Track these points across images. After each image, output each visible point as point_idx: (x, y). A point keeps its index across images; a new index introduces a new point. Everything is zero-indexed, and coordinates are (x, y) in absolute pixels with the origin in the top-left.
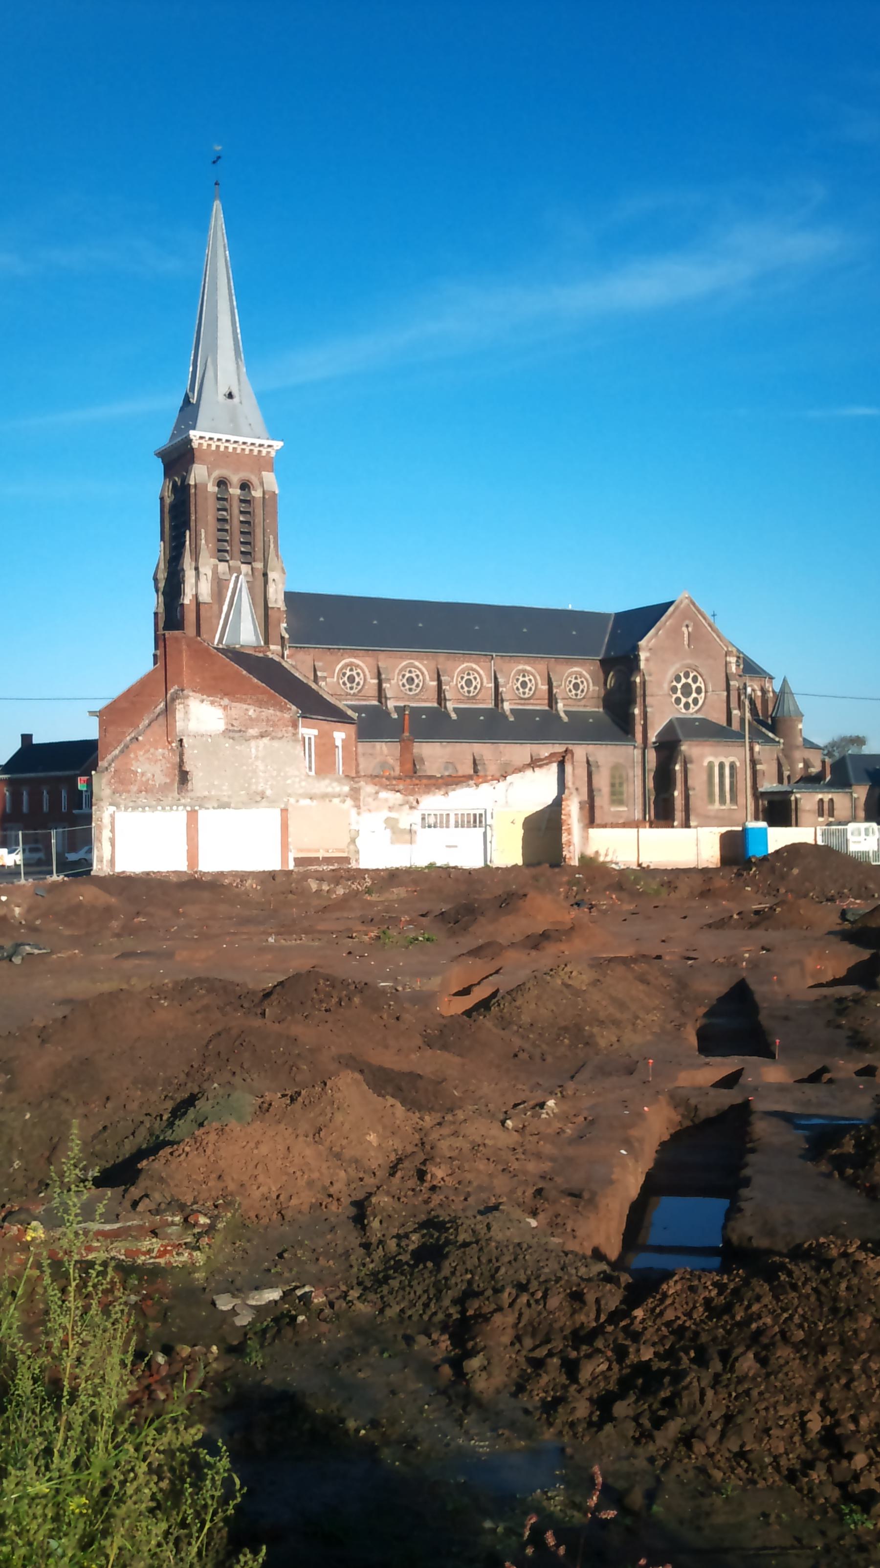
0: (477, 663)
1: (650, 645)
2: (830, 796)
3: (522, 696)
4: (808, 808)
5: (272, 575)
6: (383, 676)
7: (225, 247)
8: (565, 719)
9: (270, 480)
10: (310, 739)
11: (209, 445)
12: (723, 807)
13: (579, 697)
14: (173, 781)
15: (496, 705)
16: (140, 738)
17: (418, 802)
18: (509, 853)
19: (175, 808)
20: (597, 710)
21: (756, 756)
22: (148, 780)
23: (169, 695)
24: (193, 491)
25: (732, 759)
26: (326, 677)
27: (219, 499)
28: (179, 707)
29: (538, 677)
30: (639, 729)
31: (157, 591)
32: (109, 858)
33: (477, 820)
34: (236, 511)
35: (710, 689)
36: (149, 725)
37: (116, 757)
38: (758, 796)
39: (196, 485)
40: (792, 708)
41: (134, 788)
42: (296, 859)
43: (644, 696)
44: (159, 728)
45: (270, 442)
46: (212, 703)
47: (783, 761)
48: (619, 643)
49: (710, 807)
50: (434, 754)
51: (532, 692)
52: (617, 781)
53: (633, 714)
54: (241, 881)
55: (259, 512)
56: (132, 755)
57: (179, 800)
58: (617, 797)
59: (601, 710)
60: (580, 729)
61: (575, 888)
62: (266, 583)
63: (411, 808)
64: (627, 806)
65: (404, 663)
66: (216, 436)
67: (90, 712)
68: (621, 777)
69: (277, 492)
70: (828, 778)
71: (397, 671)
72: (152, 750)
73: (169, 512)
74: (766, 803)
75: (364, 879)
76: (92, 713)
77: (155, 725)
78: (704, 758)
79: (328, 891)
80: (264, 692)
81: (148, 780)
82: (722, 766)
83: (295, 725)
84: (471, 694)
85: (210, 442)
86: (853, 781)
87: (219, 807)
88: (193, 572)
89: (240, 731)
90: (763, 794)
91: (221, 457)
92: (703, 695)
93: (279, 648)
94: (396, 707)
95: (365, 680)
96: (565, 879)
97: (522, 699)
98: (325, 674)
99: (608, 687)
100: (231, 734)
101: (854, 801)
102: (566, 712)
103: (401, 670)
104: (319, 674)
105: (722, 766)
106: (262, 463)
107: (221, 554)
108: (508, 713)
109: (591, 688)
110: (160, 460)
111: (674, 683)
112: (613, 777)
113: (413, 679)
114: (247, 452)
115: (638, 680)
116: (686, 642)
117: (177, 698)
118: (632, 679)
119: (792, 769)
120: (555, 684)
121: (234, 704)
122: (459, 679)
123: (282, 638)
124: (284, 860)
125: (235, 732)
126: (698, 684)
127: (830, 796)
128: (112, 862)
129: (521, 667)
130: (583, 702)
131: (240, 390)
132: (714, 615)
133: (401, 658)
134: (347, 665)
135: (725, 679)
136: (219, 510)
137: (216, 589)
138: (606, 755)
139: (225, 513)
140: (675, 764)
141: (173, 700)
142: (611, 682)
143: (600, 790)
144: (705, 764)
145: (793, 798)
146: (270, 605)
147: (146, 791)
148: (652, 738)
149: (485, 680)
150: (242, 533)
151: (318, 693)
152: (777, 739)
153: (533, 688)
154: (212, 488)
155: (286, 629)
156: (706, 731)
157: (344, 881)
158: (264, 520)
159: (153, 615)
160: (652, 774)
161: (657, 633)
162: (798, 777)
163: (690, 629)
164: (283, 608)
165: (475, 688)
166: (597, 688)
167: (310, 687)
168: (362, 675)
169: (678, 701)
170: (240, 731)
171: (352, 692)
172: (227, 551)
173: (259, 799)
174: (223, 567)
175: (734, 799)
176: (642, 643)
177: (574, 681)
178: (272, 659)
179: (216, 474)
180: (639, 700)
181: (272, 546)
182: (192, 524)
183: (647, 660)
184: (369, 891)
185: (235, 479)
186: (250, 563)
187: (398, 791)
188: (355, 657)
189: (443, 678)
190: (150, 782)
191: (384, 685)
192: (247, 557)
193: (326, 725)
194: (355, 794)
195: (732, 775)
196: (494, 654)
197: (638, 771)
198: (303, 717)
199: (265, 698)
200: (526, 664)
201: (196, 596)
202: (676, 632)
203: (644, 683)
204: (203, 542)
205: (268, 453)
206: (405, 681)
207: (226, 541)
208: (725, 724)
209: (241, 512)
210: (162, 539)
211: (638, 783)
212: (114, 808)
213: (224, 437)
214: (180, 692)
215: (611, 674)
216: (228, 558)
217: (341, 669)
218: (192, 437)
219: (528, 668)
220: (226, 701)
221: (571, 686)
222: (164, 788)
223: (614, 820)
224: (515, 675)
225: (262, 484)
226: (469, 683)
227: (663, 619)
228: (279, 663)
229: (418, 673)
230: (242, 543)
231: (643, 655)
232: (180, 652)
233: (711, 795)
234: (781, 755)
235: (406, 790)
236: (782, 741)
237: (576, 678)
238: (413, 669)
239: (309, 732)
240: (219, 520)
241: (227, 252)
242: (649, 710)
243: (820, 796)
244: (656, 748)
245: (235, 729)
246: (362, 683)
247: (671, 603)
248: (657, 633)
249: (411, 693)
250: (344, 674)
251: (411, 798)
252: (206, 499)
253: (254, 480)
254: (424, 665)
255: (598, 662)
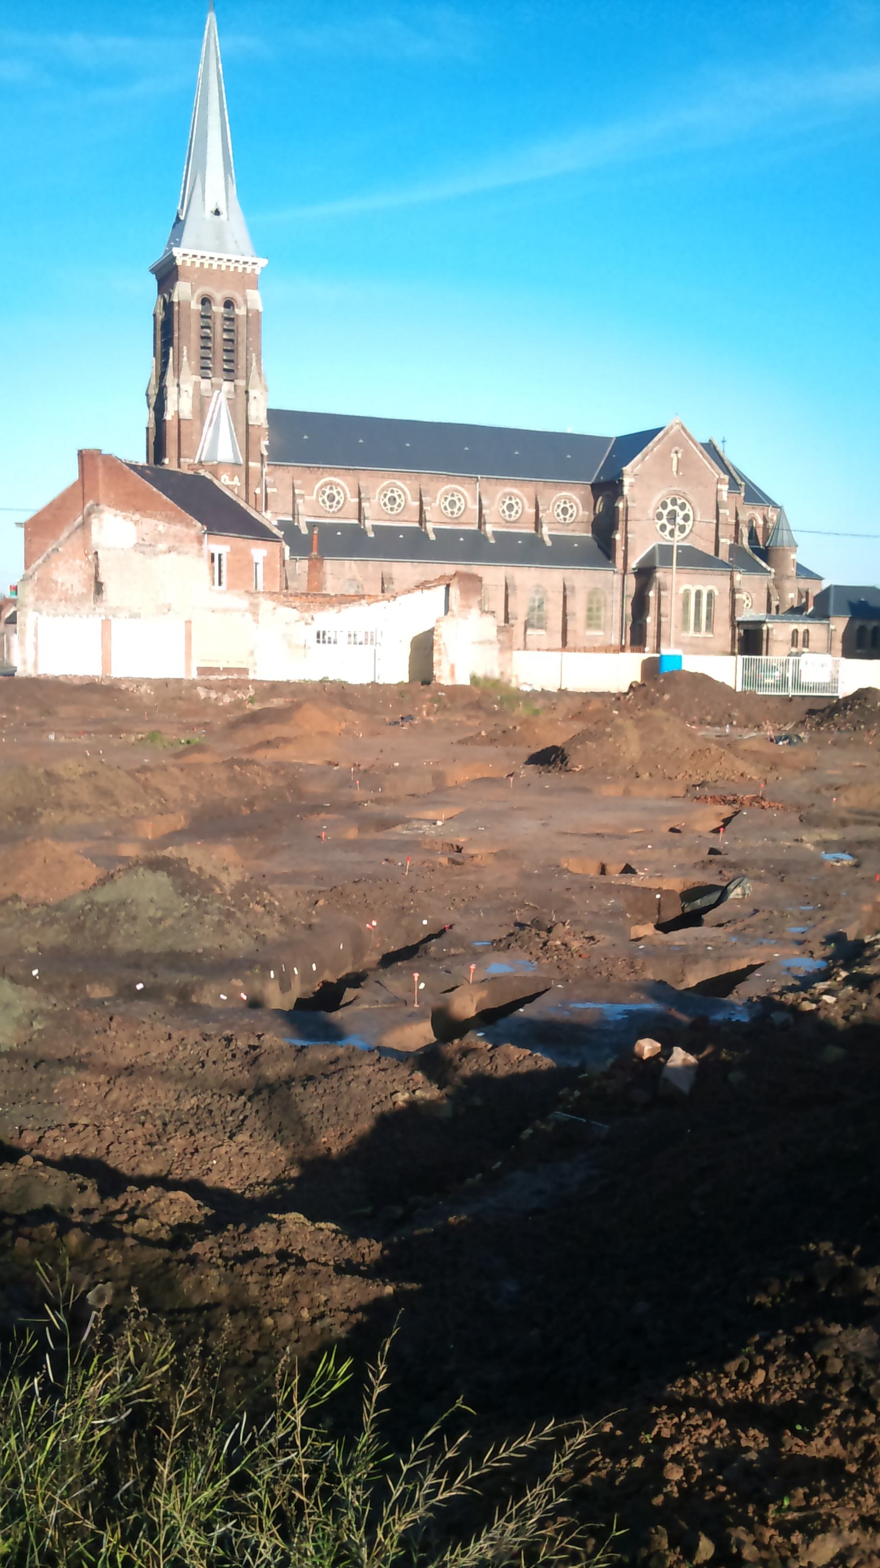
0: (462, 485)
1: (635, 471)
2: (805, 627)
3: (507, 518)
4: (780, 638)
5: (252, 393)
6: (363, 495)
7: (217, 59)
8: (549, 543)
9: (255, 299)
10: (220, 555)
11: (193, 263)
12: (698, 635)
13: (567, 521)
14: (89, 590)
15: (480, 527)
16: (60, 549)
17: (312, 619)
18: (396, 671)
19: (91, 616)
20: (586, 535)
21: (736, 586)
22: (67, 590)
23: (85, 510)
24: (176, 308)
25: (710, 587)
26: (303, 495)
27: (203, 317)
28: (95, 522)
29: (525, 501)
30: (619, 555)
31: (149, 406)
32: (33, 660)
33: (370, 639)
34: (219, 329)
35: (698, 519)
36: (68, 537)
37: (39, 566)
38: (735, 624)
39: (179, 303)
40: (785, 538)
41: (55, 597)
42: (198, 669)
43: (626, 520)
44: (76, 540)
45: (255, 260)
46: (125, 518)
47: (774, 592)
48: (604, 468)
49: (684, 634)
50: (340, 573)
51: (518, 516)
52: (595, 606)
53: (614, 539)
54: (137, 686)
55: (242, 330)
56: (53, 565)
57: (95, 609)
58: (592, 620)
59: (590, 535)
60: (561, 554)
61: (436, 705)
62: (248, 400)
63: (307, 624)
64: (604, 630)
65: (386, 483)
66: (199, 253)
67: (17, 524)
68: (599, 602)
69: (261, 310)
70: (811, 609)
71: (378, 491)
72: (71, 561)
73: (161, 330)
74: (742, 632)
75: (248, 689)
76: (18, 524)
77: (74, 538)
78: (677, 585)
79: (216, 699)
80: (172, 509)
81: (67, 590)
82: (698, 594)
83: (200, 542)
84: (455, 516)
85: (194, 259)
86: (831, 612)
87: (131, 617)
88: (176, 389)
89: (150, 545)
90: (739, 623)
91: (205, 275)
92: (690, 522)
93: (259, 465)
94: (373, 526)
95: (345, 499)
96: (428, 696)
97: (507, 522)
98: (302, 492)
99: (597, 512)
100: (142, 549)
101: (830, 632)
102: (551, 536)
103: (383, 490)
104: (297, 491)
105: (698, 594)
106: (247, 281)
107: (204, 370)
108: (490, 535)
110: (154, 276)
111: (660, 510)
112: (590, 601)
113: (395, 499)
114: (232, 269)
115: (621, 505)
116: (674, 469)
117: (94, 512)
118: (616, 505)
119: (782, 599)
120: (541, 508)
121: (145, 519)
122: (443, 500)
123: (262, 455)
124: (188, 670)
125: (144, 547)
126: (686, 512)
127: (805, 627)
128: (35, 665)
129: (508, 490)
130: (571, 527)
131: (227, 208)
132: (723, 441)
133: (383, 477)
134: (326, 484)
135: (715, 507)
136: (203, 327)
137: (198, 404)
138: (584, 579)
139: (208, 331)
140: (650, 590)
141: (89, 514)
142: (600, 507)
143: (574, 614)
144: (681, 591)
145: (765, 628)
146: (250, 423)
147: (66, 601)
148: (633, 563)
149: (469, 502)
150: (225, 350)
151: (246, 511)
152: (769, 569)
153: (520, 511)
154: (196, 306)
155: (266, 446)
156: (692, 559)
157: (230, 690)
158: (247, 338)
159: (145, 431)
160: (630, 600)
161: (643, 459)
162: (788, 607)
163: (680, 455)
164: (266, 425)
165: (459, 509)
166: (587, 513)
167: (239, 505)
168: (342, 494)
169: (663, 528)
170: (150, 545)
171: (331, 510)
172: (209, 368)
173: (166, 610)
174: (205, 384)
175: (709, 627)
176: (627, 469)
177: (562, 506)
178: (204, 477)
179: (201, 291)
180: (621, 525)
181: (254, 364)
182: (175, 341)
183: (632, 485)
184: (252, 700)
185: (219, 297)
186: (232, 381)
187: (295, 608)
188: (335, 476)
189: (424, 499)
190: (69, 591)
191: (363, 504)
192: (230, 374)
193: (241, 543)
194: (254, 609)
195: (710, 603)
196: (479, 476)
197: (618, 597)
198: (209, 534)
199: (172, 514)
200: (512, 486)
201: (178, 413)
202: (664, 457)
203: (627, 509)
204: (185, 359)
205: (253, 270)
206: (386, 500)
207: (209, 358)
208: (712, 554)
209: (225, 330)
210: (155, 355)
211: (617, 608)
212: (37, 614)
213: (208, 255)
214: (95, 507)
215: (600, 499)
216: (211, 375)
217: (321, 487)
218: (175, 254)
219: (515, 491)
220: (137, 517)
221: (559, 511)
222: (82, 598)
223: (587, 644)
224: (501, 498)
225: (246, 301)
226: (452, 504)
227: (651, 444)
228: (211, 482)
229: (400, 492)
230: (225, 361)
231: (627, 481)
232: (96, 469)
233: (685, 621)
234: (771, 585)
235: (302, 606)
236: (773, 571)
237: (565, 503)
238: (395, 489)
239: (221, 546)
240: (202, 338)
241: (220, 66)
242: (629, 536)
243: (795, 626)
244: (635, 573)
245: (146, 543)
246: (342, 501)
247: (661, 429)
248: (643, 459)
249: (392, 513)
250: (324, 493)
251: (307, 615)
252: (189, 317)
253: (239, 298)
254: (407, 485)
255: (589, 487)
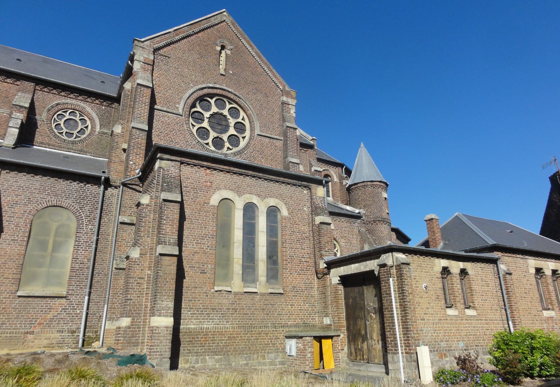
25: (272, 202)
82: (250, 209)
105: (250, 210)
109: (98, 129)
144: (215, 200)
